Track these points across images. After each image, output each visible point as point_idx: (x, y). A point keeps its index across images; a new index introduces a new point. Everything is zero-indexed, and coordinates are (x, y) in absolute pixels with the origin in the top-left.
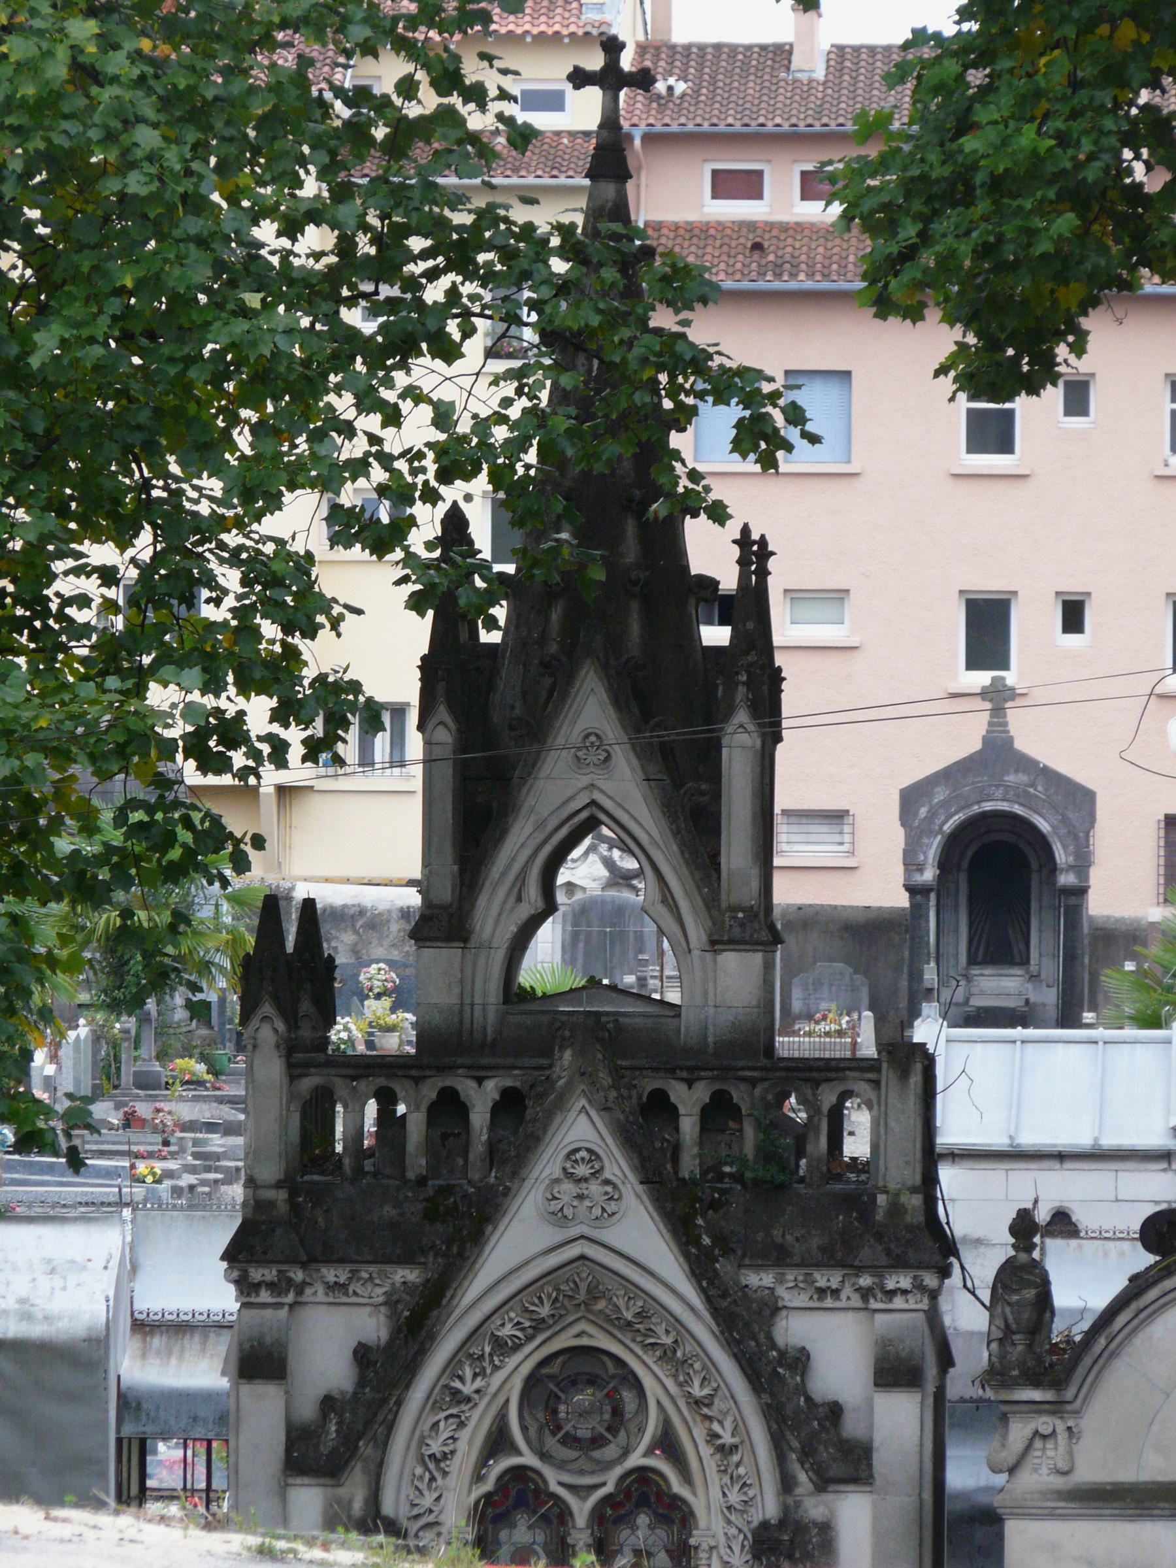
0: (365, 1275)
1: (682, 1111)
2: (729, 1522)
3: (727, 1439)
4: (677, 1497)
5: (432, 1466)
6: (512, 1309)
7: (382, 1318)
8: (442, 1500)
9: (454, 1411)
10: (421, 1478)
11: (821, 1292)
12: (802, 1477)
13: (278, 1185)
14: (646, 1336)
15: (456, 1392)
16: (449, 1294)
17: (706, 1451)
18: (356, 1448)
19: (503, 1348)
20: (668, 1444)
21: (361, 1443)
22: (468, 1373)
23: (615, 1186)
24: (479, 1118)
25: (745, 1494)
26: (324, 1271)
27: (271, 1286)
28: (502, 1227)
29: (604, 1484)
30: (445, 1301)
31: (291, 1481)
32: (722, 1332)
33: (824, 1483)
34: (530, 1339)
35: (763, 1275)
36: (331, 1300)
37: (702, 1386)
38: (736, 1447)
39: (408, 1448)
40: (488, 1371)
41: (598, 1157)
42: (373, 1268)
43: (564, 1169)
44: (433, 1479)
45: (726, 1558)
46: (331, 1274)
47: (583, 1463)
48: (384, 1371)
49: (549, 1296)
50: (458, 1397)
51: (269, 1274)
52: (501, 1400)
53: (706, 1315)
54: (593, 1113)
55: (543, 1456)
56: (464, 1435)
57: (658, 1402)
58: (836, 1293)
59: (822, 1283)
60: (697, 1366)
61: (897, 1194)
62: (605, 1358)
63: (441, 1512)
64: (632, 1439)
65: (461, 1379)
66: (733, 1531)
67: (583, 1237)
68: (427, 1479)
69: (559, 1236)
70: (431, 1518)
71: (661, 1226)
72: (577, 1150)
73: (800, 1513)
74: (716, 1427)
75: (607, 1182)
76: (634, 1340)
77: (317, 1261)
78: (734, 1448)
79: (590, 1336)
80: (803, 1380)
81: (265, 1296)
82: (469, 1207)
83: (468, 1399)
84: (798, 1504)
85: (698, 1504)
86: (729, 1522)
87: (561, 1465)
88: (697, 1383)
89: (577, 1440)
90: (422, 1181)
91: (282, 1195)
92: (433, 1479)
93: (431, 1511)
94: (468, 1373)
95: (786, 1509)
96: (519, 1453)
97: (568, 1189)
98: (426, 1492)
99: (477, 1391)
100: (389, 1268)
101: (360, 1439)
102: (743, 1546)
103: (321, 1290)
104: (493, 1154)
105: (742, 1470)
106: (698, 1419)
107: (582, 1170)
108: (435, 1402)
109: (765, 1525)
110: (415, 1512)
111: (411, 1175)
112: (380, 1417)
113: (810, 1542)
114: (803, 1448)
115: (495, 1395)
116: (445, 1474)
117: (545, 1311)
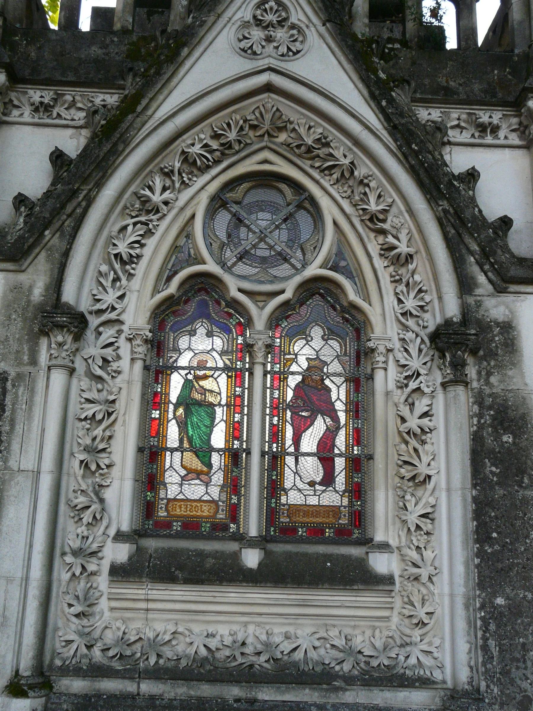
0: (69, 98)
2: (406, 328)
3: (403, 248)
5: (117, 266)
6: (202, 131)
8: (126, 299)
9: (143, 219)
10: (106, 275)
11: (482, 128)
12: (482, 279)
14: (326, 160)
15: (145, 201)
18: (41, 235)
19: (193, 166)
21: (47, 233)
23: (300, 31)
25: (422, 299)
26: (31, 92)
28: (196, 54)
29: (283, 292)
30: (139, 108)
32: (400, 148)
34: (217, 162)
35: (431, 110)
36: (36, 120)
37: (377, 204)
38: (411, 256)
40: (177, 185)
43: (255, 17)
44: (117, 279)
45: (403, 362)
46: (36, 95)
47: (262, 277)
50: (147, 207)
52: (188, 213)
55: (223, 264)
57: (335, 223)
58: (495, 130)
62: (283, 186)
63: (123, 311)
64: (309, 256)
65: (150, 188)
68: (111, 278)
69: (248, 65)
70: (113, 316)
71: (342, 59)
73: (482, 312)
75: (293, 27)
76: (312, 167)
77: (25, 81)
78: (410, 257)
79: (270, 163)
80: (474, 194)
82: (168, 40)
84: (479, 304)
88: (372, 199)
89: (314, 167)
92: (117, 279)
93: (114, 309)
97: (257, 34)
98: (110, 290)
99: (166, 203)
101: (46, 228)
102: (420, 351)
103: (27, 110)
105: (417, 278)
106: (372, 235)
107: (270, 17)
108: (125, 207)
110: (98, 306)
112: (69, 209)
113: (493, 340)
114: (483, 250)
115: (182, 209)
116: (130, 276)
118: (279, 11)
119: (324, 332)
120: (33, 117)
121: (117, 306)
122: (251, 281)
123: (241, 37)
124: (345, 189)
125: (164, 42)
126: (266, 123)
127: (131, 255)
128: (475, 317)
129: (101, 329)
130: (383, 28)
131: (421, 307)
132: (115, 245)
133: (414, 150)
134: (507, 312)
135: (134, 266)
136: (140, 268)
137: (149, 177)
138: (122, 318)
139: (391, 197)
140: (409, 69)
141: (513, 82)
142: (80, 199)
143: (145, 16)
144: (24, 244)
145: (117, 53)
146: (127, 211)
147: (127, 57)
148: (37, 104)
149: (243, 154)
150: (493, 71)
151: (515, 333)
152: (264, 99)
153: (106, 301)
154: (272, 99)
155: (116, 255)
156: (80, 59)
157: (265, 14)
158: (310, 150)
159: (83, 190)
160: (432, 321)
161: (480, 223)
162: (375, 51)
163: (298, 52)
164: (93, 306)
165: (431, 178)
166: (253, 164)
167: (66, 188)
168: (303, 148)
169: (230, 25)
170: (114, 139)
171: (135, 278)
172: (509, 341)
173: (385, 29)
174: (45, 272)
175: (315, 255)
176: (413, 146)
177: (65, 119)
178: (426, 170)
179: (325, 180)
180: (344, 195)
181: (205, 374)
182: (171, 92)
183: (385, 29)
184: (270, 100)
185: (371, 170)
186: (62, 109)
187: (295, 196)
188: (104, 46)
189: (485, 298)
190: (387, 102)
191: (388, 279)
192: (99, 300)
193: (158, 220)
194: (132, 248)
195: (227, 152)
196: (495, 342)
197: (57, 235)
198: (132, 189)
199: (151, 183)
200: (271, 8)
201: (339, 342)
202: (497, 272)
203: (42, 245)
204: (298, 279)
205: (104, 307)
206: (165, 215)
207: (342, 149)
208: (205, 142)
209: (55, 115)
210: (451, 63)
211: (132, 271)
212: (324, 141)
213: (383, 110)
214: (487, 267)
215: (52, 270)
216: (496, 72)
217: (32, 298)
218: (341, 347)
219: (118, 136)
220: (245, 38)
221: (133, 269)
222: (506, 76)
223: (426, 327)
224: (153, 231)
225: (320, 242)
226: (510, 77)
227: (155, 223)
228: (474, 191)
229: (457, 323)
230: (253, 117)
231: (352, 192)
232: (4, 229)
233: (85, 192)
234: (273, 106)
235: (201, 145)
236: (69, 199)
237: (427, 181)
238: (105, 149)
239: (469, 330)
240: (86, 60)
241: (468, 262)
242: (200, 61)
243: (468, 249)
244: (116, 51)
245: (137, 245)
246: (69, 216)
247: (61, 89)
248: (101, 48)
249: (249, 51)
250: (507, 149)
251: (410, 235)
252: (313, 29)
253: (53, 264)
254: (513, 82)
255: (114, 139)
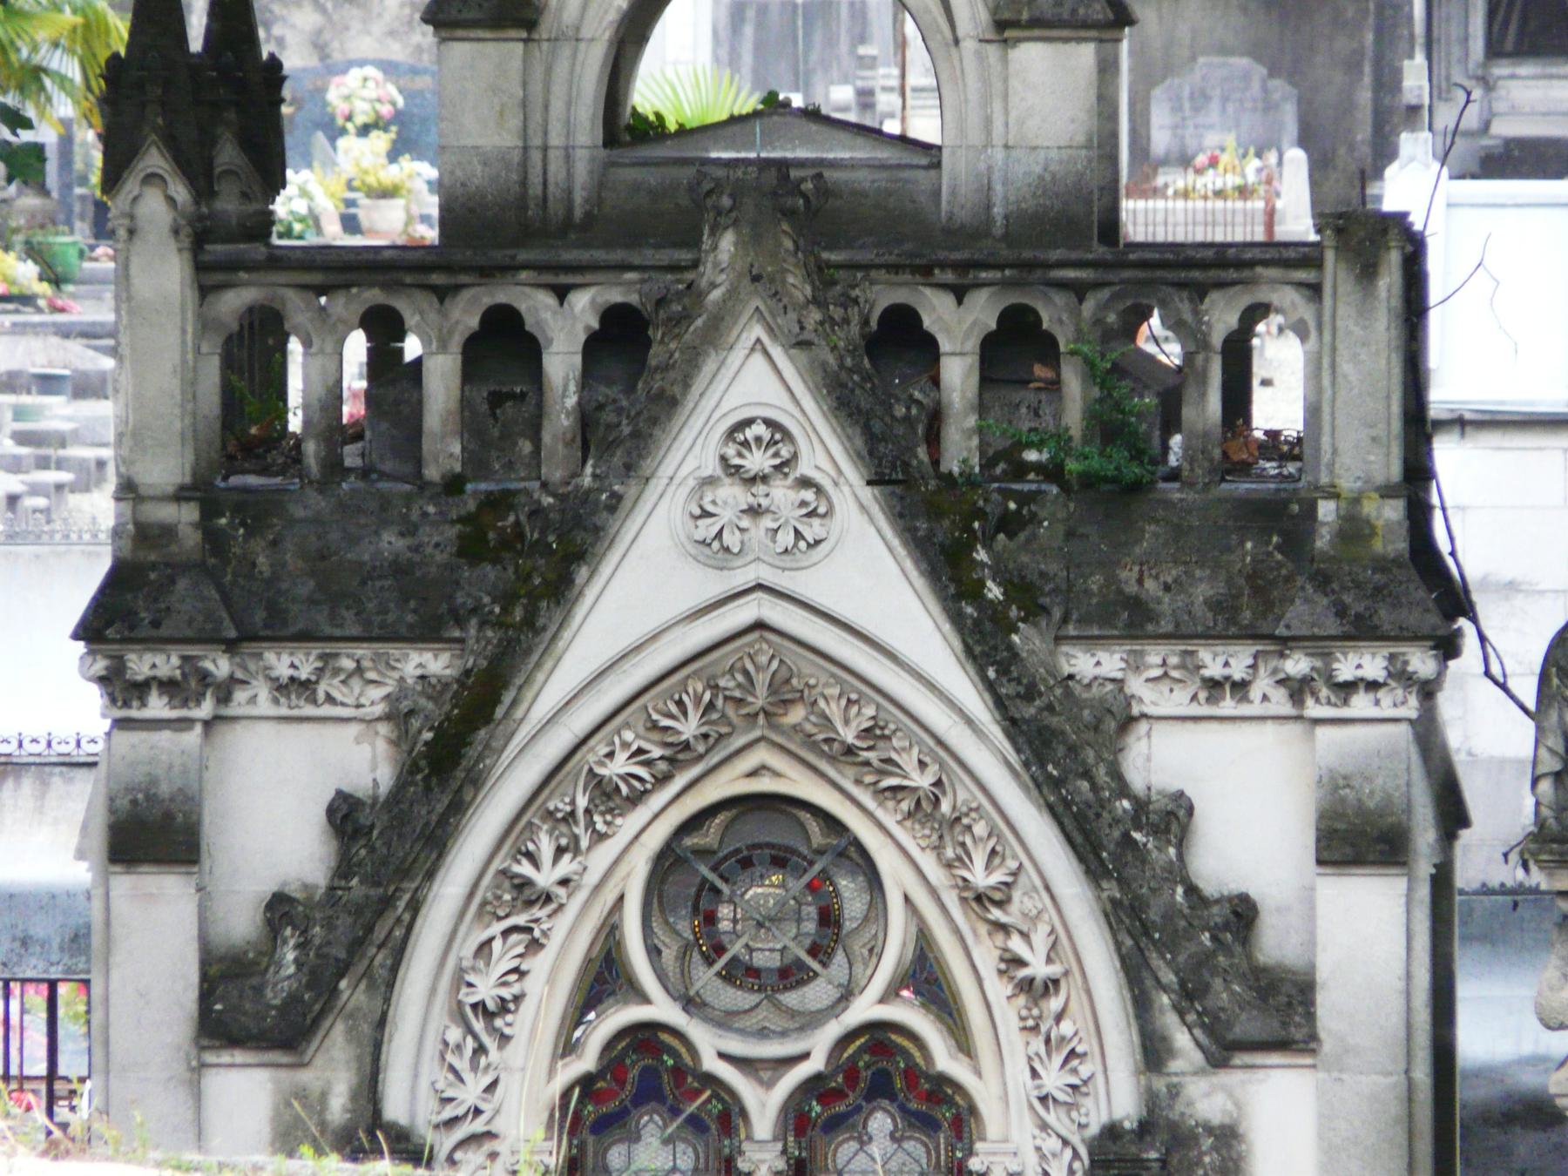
0: (348, 664)
1: (945, 345)
2: (1044, 1126)
3: (1039, 968)
4: (944, 1080)
5: (479, 1025)
6: (627, 725)
7: (382, 746)
9: (520, 920)
11: (1214, 687)
12: (1182, 1039)
13: (180, 495)
14: (883, 773)
15: (524, 884)
16: (507, 698)
17: (999, 990)
18: (334, 992)
20: (925, 978)
21: (343, 984)
22: (546, 847)
23: (819, 490)
24: (562, 364)
25: (1074, 1071)
26: (270, 657)
27: (169, 687)
29: (805, 1056)
30: (499, 712)
31: (210, 1058)
33: (1223, 1050)
34: (662, 780)
35: (1102, 656)
36: (284, 711)
37: (988, 866)
38: (1056, 982)
39: (433, 991)
40: (584, 843)
41: (787, 436)
42: (363, 651)
43: (723, 459)
46: (283, 662)
48: (385, 844)
49: (698, 699)
51: (166, 664)
52: (609, 896)
53: (996, 732)
54: (777, 352)
55: (691, 1004)
56: (538, 965)
57: (907, 899)
59: (1214, 670)
60: (980, 829)
61: (1356, 501)
62: (805, 816)
63: (497, 1112)
64: (858, 969)
65: (532, 858)
66: (1052, 1144)
67: (760, 587)
68: (468, 1052)
70: (478, 1126)
72: (749, 422)
73: (1180, 1107)
74: (1016, 945)
75: (805, 483)
76: (858, 782)
79: (777, 774)
81: (157, 706)
82: (543, 533)
83: (548, 898)
84: (1174, 1092)
85: (983, 1092)
86: (1044, 1126)
87: (724, 1021)
88: (979, 858)
90: (453, 485)
91: (188, 514)
92: (481, 1049)
93: (478, 1112)
94: (546, 847)
95: (1151, 1100)
96: (645, 999)
97: (731, 496)
98: (467, 1076)
99: (564, 882)
100: (394, 650)
101: (341, 976)
103: (263, 692)
104: (590, 432)
105: (1066, 1028)
106: (983, 929)
107: (758, 461)
108: (484, 903)
109: (1112, 1132)
110: (449, 1112)
111: (432, 473)
112: (380, 933)
115: (598, 888)
116: (504, 1039)
117: (689, 728)
118: (776, 443)
119: (896, 1126)
120: (276, 701)
121: (482, 1106)
122: (742, 1032)
123: (697, 512)
124: (927, 832)
125: (536, 536)
126: (758, 692)
127: (503, 1000)
128: (1167, 1118)
129: (458, 1156)
130: (1018, 406)
131: (1074, 1087)
132: (470, 985)
133: (1050, 776)
134: (1230, 1106)
135: (509, 1018)
136: (519, 1023)
137: (527, 834)
138: (493, 1128)
139: (1015, 857)
140: (1061, 549)
141: (1284, 572)
142: (400, 910)
143: (485, 407)
144: (305, 1015)
145: (437, 545)
146: (489, 908)
147: (461, 553)
148: (284, 680)
149: (715, 758)
150: (1242, 543)
151: (1244, 1147)
152: (750, 645)
153: (463, 1102)
154: (767, 641)
155: (474, 1006)
156: (361, 564)
157: (745, 452)
158: (850, 751)
159: (404, 891)
160: (1096, 1117)
161: (1183, 923)
162: (979, 534)
163: (817, 542)
164: (439, 1113)
165: (1086, 835)
166: (738, 778)
167: (372, 892)
168: (836, 745)
169: (672, 488)
170: (455, 785)
171: (513, 1042)
172: (1230, 1164)
173: (1024, 410)
174: (348, 1062)
175: (869, 972)
176: (1050, 768)
177: (343, 704)
178: (1075, 817)
179: (886, 809)
180: (924, 844)
181: (614, 1048)
182: (560, 659)
183: (1024, 410)
184: (765, 646)
185: (975, 798)
186: (336, 681)
187: (828, 836)
188: (409, 530)
189: (1188, 1079)
190: (997, 671)
191: (1015, 1023)
192: (450, 1100)
193: (549, 916)
194: (505, 984)
195: (681, 756)
196: (1204, 1166)
197: (362, 986)
198: (497, 864)
199: (531, 847)
200: (758, 439)
201: (926, 1145)
202: (1209, 1030)
203: (336, 1011)
204: (832, 1030)
205: (460, 1111)
206: (561, 906)
207: (915, 751)
208: (634, 747)
209: (321, 696)
210: (1153, 527)
211: (507, 1031)
212: (878, 732)
213: (990, 686)
214: (1191, 1017)
215: (359, 1058)
216: (1249, 545)
217: (329, 1117)
218: (928, 1153)
219: (463, 775)
220: (706, 514)
221: (509, 1025)
222: (1270, 554)
223: (1085, 1126)
224: (543, 941)
225: (880, 936)
226: (1279, 557)
227: (545, 926)
228: (1180, 846)
229: (1133, 1131)
230: (732, 684)
231: (941, 837)
232: (246, 953)
233: (407, 896)
234: (773, 657)
235: (627, 755)
236: (380, 914)
237: (1079, 839)
238: (440, 808)
239: (1147, 1151)
240: (374, 568)
241: (1156, 1006)
242: (614, 583)
243: (1157, 980)
244: (436, 539)
245: (513, 977)
246: (380, 947)
247: (329, 648)
248: (402, 535)
249: (716, 545)
250: (1269, 722)
251: (1053, 937)
252: (846, 489)
253: (360, 1045)
254: (1284, 572)
255: (455, 785)
